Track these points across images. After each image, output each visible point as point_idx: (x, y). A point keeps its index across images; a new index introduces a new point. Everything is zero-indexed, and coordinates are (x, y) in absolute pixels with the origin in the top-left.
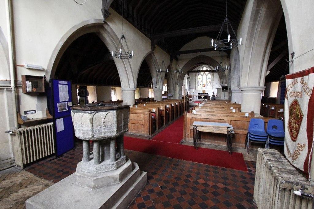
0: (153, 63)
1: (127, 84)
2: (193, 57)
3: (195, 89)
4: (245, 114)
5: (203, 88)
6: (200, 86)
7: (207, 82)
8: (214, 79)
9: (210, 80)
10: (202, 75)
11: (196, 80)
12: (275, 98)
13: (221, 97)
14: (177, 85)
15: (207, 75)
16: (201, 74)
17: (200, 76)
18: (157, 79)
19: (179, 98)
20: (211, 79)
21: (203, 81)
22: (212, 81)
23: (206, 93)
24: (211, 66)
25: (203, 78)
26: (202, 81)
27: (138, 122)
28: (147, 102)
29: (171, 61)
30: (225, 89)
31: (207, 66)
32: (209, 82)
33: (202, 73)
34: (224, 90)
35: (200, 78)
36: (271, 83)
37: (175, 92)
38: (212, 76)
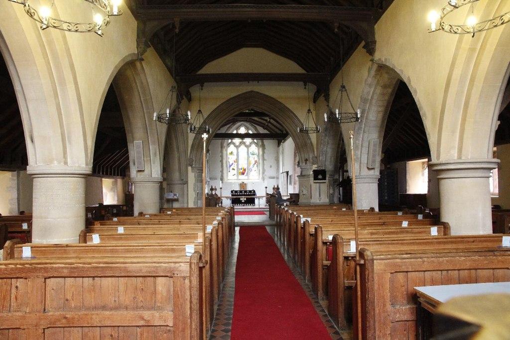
0: (136, 93)
1: (56, 149)
2: (233, 95)
3: (222, 179)
4: (501, 241)
5: (241, 177)
6: (233, 172)
7: (249, 163)
8: (265, 155)
9: (256, 159)
10: (237, 147)
11: (222, 156)
12: (425, 194)
13: (311, 198)
14: (190, 168)
15: (248, 147)
16: (234, 144)
17: (232, 148)
18: (146, 143)
19: (195, 203)
20: (258, 156)
21: (240, 162)
22: (261, 161)
23: (249, 188)
24: (257, 126)
25: (240, 154)
26: (237, 161)
27: (143, 319)
28: (115, 219)
29: (179, 102)
30: (320, 177)
31: (248, 124)
32: (253, 162)
33: (237, 141)
34: (319, 179)
35: (232, 153)
36: (407, 162)
37: (185, 186)
38: (261, 149)
